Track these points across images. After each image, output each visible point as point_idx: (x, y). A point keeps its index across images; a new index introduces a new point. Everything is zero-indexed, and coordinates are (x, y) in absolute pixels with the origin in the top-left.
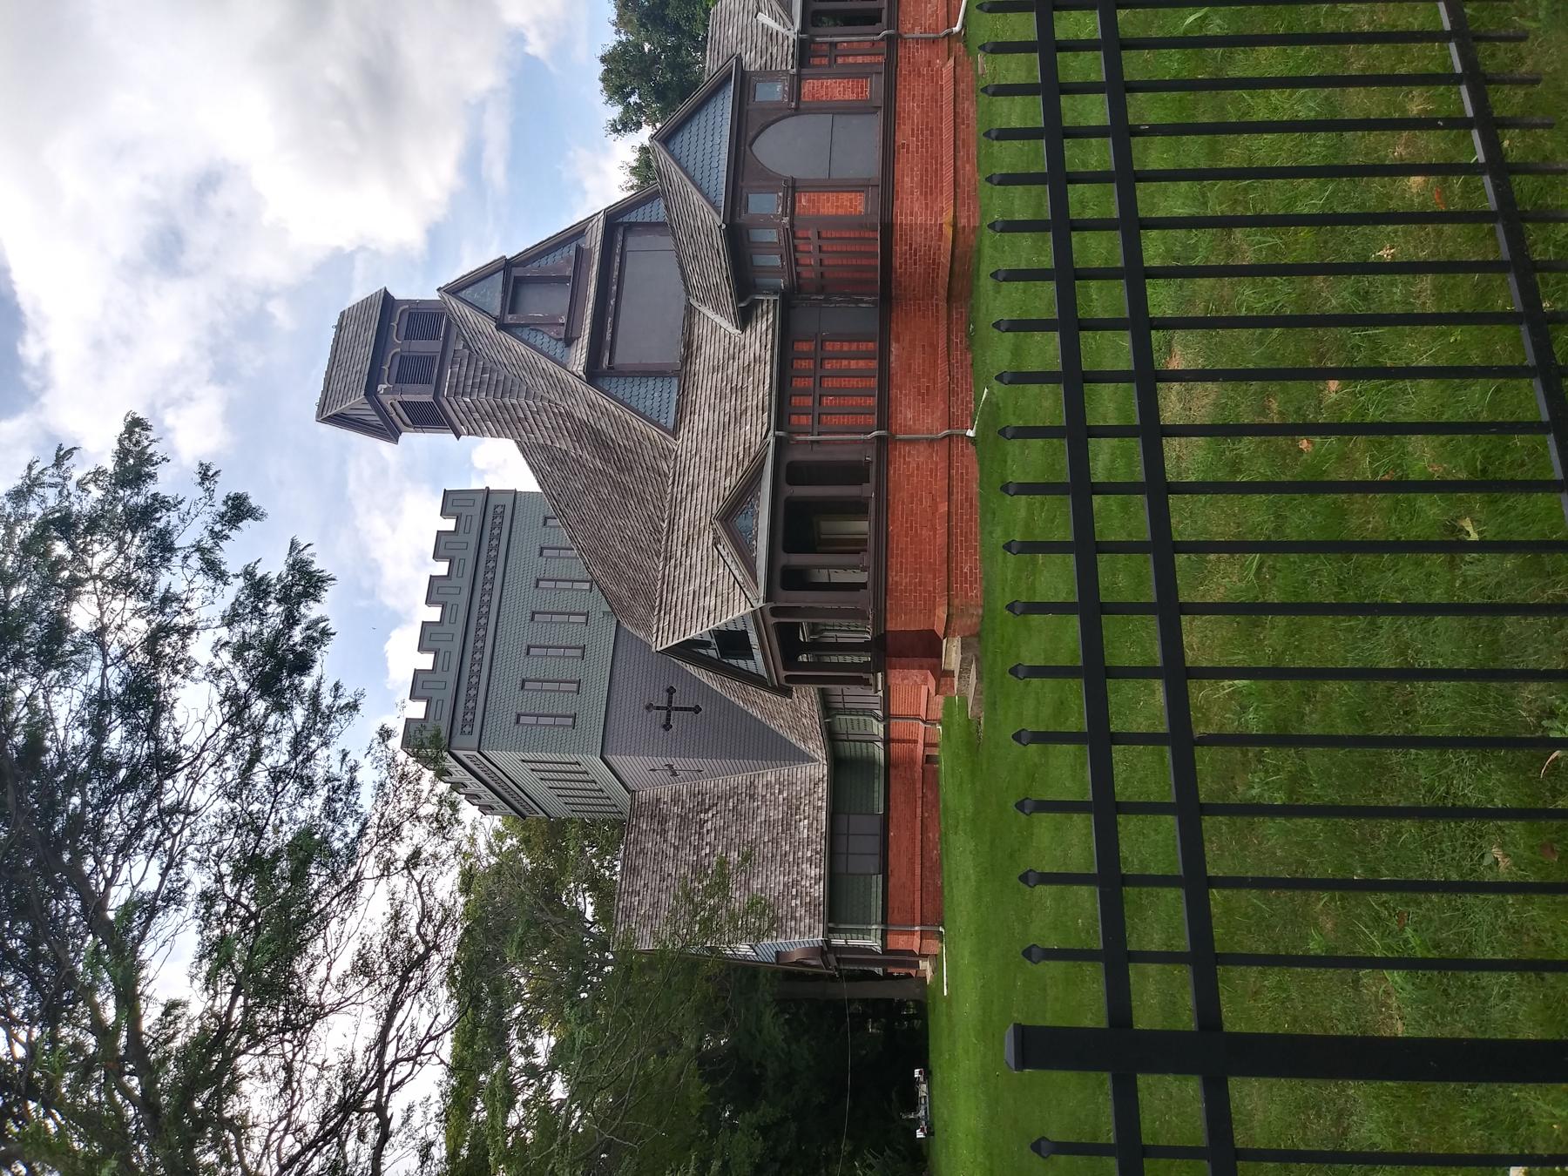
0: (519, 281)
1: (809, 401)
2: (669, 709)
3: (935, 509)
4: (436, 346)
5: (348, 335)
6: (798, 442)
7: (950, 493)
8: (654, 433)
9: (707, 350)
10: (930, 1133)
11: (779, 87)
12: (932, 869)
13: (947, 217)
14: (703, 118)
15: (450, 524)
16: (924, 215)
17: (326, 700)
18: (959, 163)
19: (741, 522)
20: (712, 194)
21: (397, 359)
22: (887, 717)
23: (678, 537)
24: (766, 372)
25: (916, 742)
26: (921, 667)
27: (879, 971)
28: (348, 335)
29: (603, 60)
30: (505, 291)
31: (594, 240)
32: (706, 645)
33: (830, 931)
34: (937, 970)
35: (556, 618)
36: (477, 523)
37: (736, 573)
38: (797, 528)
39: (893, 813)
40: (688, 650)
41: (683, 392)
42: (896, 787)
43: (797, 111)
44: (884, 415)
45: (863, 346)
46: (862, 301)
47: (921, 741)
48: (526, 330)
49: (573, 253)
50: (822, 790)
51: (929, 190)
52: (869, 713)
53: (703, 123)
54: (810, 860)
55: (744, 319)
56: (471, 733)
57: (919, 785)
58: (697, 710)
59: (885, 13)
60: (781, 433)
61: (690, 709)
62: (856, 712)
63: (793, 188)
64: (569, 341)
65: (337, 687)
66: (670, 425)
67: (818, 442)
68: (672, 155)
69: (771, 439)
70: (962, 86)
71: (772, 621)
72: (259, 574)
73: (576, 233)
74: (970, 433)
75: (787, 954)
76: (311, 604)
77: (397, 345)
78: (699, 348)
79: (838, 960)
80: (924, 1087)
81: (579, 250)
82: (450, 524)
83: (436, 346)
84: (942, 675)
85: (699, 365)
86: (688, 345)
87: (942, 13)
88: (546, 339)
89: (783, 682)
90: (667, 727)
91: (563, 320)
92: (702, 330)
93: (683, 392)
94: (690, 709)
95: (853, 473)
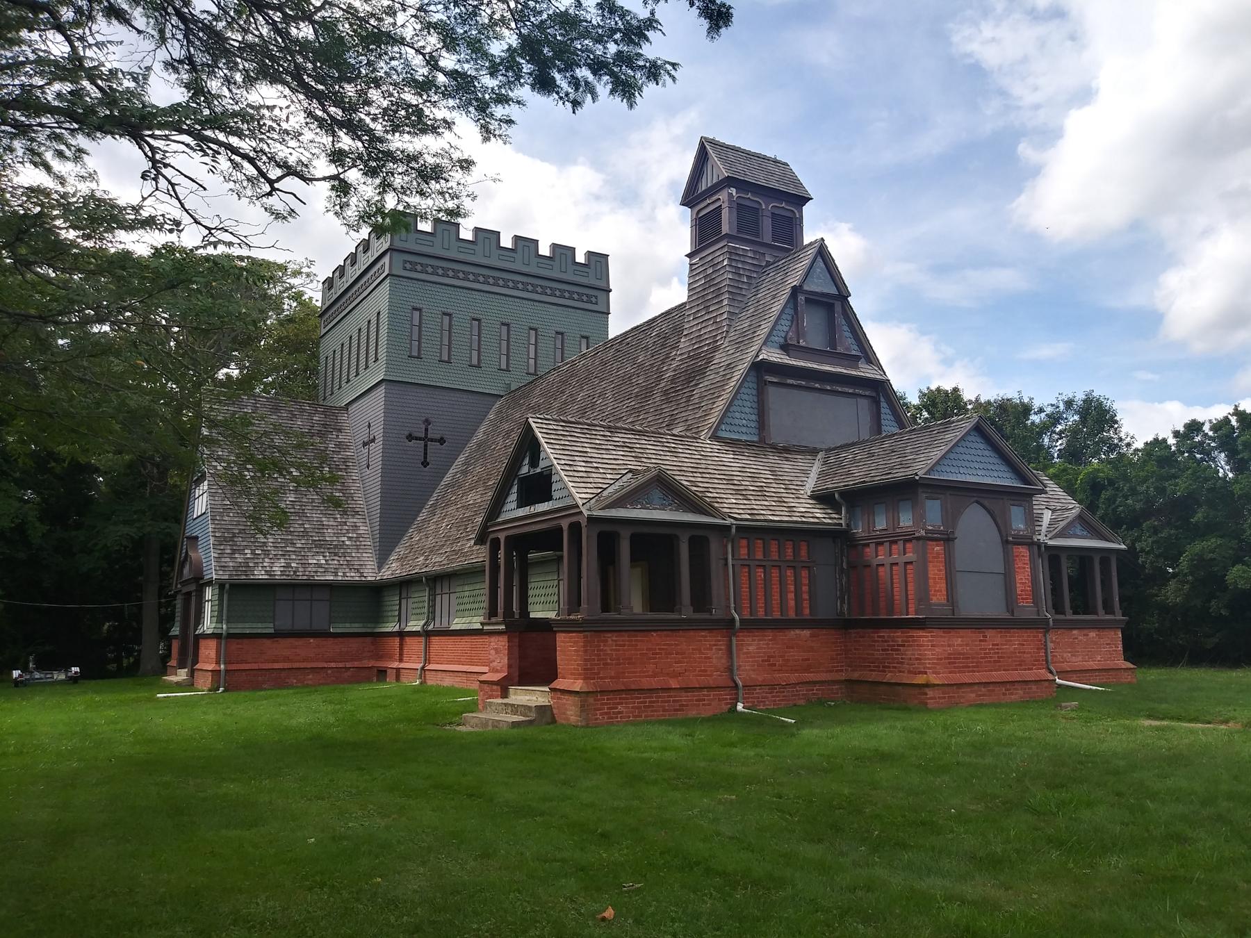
0: (829, 308)
1: (760, 556)
2: (426, 439)
3: (676, 675)
4: (767, 239)
5: (771, 167)
6: (726, 546)
7: (686, 689)
8: (713, 419)
9: (787, 466)
10: (17, 683)
11: (1022, 526)
12: (278, 680)
13: (933, 679)
14: (996, 461)
15: (580, 258)
16: (930, 654)
17: (499, 111)
18: (976, 687)
19: (656, 494)
20: (939, 468)
21: (756, 206)
22: (427, 634)
23: (628, 438)
24: (779, 516)
25: (401, 660)
26: (510, 666)
27: (175, 631)
28: (771, 167)
29: (956, 390)
30: (823, 295)
31: (865, 371)
32: (534, 462)
33: (221, 585)
34: (179, 686)
35: (504, 344)
36: (578, 281)
37: (610, 490)
38: (653, 545)
39: (330, 641)
40: (529, 446)
41: (748, 444)
42: (354, 644)
43: (1005, 542)
44: (753, 625)
45: (806, 604)
46: (842, 602)
47: (402, 665)
48: (792, 312)
49: (854, 353)
50: (353, 576)
51: (953, 661)
52: (431, 616)
53: (992, 460)
54: (288, 566)
55: (822, 498)
56: (405, 269)
57: (356, 664)
58: (425, 464)
59: (705, 616)
60: (734, 530)
61: (425, 458)
62: (432, 607)
63: (947, 539)
64: (785, 348)
65: (510, 122)
66: (722, 434)
67: (726, 564)
68: (968, 433)
69: (729, 521)
70: (1034, 687)
71: (565, 524)
72: (650, 34)
73: (869, 357)
74: (740, 707)
75: (196, 548)
76: (610, 86)
77: (767, 206)
78: (787, 459)
79: (189, 594)
80: (63, 677)
81: (857, 358)
82: (580, 258)
83: (767, 239)
84: (503, 687)
85: (773, 459)
86: (786, 450)
87: (1066, 666)
88: (786, 329)
89: (492, 536)
90: (410, 437)
91: (802, 343)
92: (801, 461)
93: (748, 444)
94: (425, 458)
95: (701, 599)
